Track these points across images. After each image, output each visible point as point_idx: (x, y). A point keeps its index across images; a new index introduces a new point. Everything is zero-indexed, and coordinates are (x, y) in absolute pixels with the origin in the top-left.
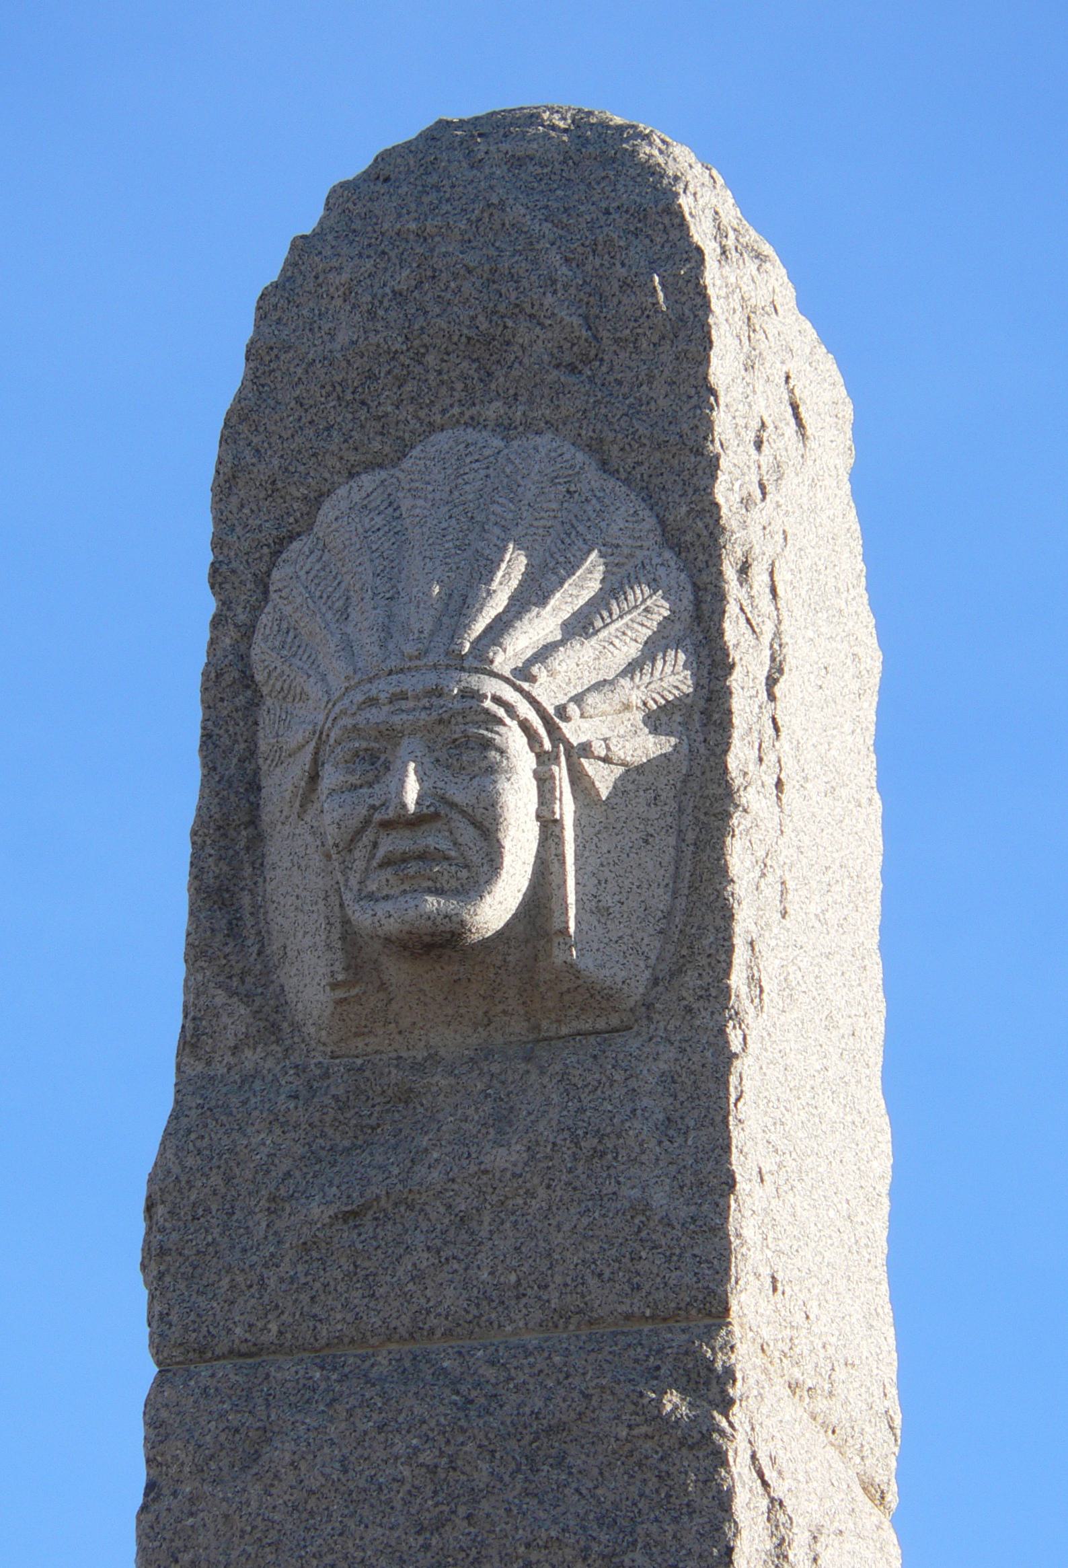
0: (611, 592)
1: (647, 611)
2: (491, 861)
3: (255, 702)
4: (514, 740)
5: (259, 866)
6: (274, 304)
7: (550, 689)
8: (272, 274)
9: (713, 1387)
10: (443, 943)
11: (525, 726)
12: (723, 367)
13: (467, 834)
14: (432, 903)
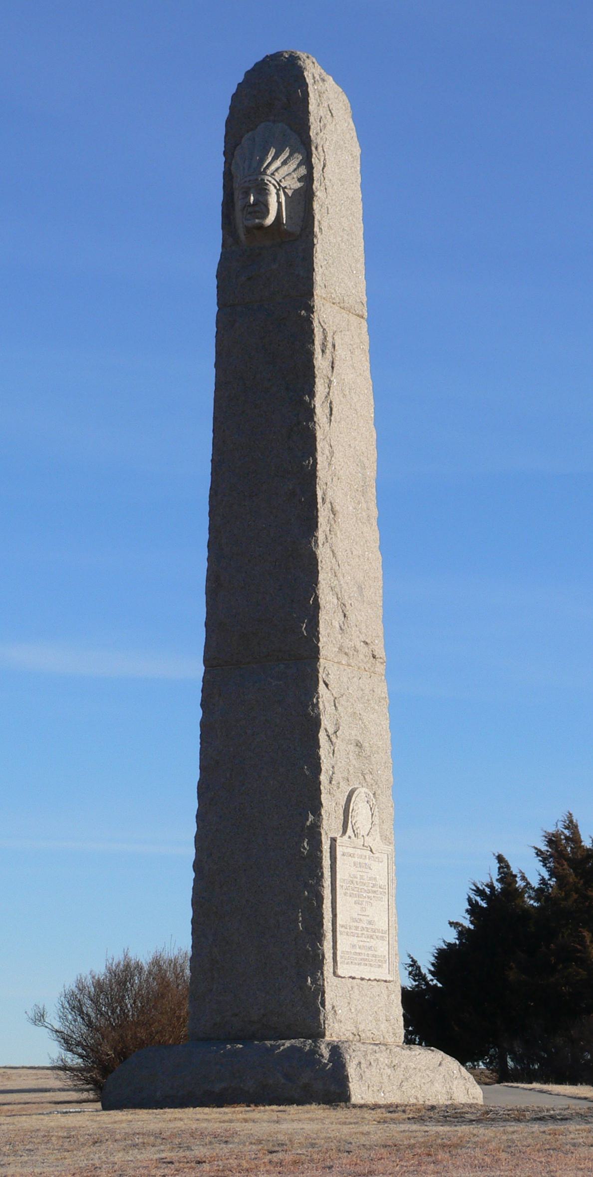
0: (291, 155)
1: (298, 157)
2: (267, 212)
3: (232, 178)
4: (272, 188)
5: (234, 210)
6: (235, 97)
7: (278, 176)
8: (234, 91)
9: (310, 309)
10: (261, 227)
11: (274, 185)
12: (312, 108)
13: (262, 206)
14: (257, 221)
